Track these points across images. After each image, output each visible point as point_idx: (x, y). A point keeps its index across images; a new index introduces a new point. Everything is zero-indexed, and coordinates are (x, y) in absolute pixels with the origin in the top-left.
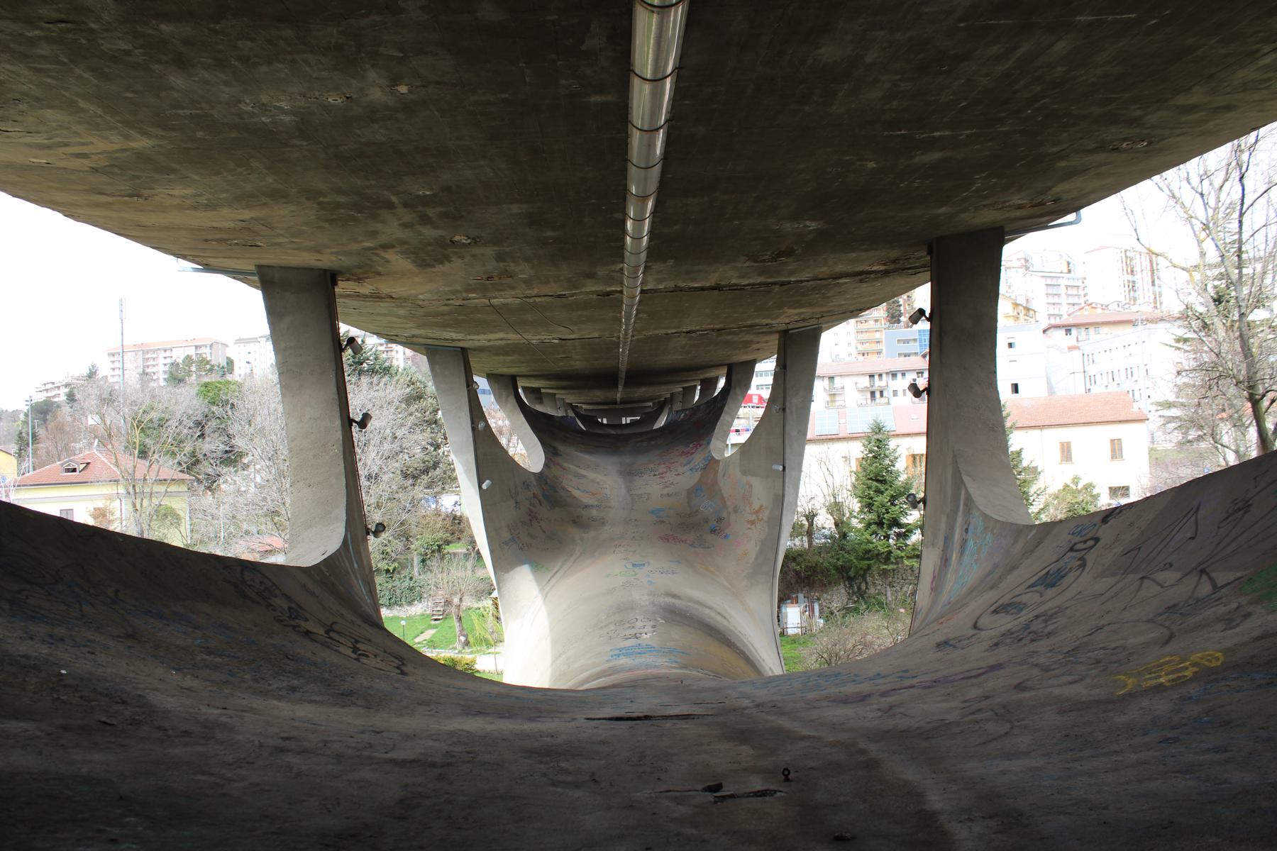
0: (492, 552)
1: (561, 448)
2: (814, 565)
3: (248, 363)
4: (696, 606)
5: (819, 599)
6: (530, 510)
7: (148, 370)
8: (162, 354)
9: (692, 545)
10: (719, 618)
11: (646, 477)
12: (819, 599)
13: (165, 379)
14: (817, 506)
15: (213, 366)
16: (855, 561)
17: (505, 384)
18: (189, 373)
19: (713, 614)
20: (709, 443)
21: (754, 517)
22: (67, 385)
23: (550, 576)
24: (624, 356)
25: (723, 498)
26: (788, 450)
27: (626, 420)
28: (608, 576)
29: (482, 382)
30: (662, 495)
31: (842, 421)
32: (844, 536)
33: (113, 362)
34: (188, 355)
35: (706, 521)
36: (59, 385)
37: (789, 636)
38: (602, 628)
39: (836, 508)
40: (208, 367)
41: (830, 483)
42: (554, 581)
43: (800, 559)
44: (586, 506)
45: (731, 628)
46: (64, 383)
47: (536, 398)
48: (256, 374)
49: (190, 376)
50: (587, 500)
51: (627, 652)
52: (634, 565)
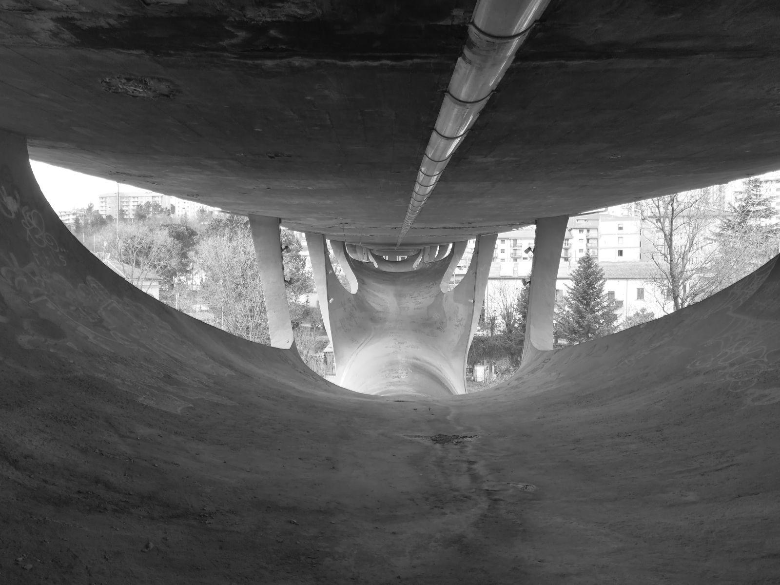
0: (332, 333)
1: (367, 280)
2: (493, 346)
3: (184, 208)
4: (427, 365)
5: (495, 364)
6: (351, 313)
7: (124, 209)
8: (132, 200)
9: (428, 335)
10: (438, 371)
11: (407, 298)
12: (495, 364)
13: (133, 214)
14: (497, 314)
15: (163, 209)
16: (514, 345)
17: (341, 246)
18: (148, 212)
19: (435, 369)
20: (440, 283)
21: (458, 323)
22: (74, 214)
23: (359, 345)
24: (400, 240)
25: (444, 312)
26: (476, 293)
27: (399, 258)
28: (386, 347)
29: (328, 242)
30: (415, 308)
31: (516, 269)
32: (510, 331)
33: (102, 202)
34: (148, 202)
35: (436, 323)
36: (69, 213)
37: (478, 382)
38: (383, 372)
39: (508, 316)
40: (160, 209)
41: (505, 303)
42: (360, 348)
43: (486, 342)
44: (377, 312)
45: (443, 376)
46: (73, 212)
47: (353, 250)
48: (188, 215)
49: (149, 213)
50: (378, 308)
51: (392, 384)
52: (399, 343)
